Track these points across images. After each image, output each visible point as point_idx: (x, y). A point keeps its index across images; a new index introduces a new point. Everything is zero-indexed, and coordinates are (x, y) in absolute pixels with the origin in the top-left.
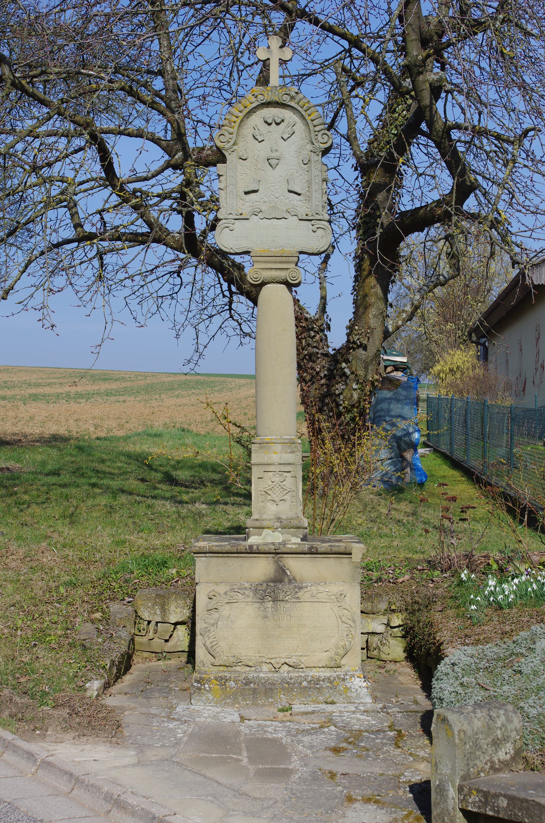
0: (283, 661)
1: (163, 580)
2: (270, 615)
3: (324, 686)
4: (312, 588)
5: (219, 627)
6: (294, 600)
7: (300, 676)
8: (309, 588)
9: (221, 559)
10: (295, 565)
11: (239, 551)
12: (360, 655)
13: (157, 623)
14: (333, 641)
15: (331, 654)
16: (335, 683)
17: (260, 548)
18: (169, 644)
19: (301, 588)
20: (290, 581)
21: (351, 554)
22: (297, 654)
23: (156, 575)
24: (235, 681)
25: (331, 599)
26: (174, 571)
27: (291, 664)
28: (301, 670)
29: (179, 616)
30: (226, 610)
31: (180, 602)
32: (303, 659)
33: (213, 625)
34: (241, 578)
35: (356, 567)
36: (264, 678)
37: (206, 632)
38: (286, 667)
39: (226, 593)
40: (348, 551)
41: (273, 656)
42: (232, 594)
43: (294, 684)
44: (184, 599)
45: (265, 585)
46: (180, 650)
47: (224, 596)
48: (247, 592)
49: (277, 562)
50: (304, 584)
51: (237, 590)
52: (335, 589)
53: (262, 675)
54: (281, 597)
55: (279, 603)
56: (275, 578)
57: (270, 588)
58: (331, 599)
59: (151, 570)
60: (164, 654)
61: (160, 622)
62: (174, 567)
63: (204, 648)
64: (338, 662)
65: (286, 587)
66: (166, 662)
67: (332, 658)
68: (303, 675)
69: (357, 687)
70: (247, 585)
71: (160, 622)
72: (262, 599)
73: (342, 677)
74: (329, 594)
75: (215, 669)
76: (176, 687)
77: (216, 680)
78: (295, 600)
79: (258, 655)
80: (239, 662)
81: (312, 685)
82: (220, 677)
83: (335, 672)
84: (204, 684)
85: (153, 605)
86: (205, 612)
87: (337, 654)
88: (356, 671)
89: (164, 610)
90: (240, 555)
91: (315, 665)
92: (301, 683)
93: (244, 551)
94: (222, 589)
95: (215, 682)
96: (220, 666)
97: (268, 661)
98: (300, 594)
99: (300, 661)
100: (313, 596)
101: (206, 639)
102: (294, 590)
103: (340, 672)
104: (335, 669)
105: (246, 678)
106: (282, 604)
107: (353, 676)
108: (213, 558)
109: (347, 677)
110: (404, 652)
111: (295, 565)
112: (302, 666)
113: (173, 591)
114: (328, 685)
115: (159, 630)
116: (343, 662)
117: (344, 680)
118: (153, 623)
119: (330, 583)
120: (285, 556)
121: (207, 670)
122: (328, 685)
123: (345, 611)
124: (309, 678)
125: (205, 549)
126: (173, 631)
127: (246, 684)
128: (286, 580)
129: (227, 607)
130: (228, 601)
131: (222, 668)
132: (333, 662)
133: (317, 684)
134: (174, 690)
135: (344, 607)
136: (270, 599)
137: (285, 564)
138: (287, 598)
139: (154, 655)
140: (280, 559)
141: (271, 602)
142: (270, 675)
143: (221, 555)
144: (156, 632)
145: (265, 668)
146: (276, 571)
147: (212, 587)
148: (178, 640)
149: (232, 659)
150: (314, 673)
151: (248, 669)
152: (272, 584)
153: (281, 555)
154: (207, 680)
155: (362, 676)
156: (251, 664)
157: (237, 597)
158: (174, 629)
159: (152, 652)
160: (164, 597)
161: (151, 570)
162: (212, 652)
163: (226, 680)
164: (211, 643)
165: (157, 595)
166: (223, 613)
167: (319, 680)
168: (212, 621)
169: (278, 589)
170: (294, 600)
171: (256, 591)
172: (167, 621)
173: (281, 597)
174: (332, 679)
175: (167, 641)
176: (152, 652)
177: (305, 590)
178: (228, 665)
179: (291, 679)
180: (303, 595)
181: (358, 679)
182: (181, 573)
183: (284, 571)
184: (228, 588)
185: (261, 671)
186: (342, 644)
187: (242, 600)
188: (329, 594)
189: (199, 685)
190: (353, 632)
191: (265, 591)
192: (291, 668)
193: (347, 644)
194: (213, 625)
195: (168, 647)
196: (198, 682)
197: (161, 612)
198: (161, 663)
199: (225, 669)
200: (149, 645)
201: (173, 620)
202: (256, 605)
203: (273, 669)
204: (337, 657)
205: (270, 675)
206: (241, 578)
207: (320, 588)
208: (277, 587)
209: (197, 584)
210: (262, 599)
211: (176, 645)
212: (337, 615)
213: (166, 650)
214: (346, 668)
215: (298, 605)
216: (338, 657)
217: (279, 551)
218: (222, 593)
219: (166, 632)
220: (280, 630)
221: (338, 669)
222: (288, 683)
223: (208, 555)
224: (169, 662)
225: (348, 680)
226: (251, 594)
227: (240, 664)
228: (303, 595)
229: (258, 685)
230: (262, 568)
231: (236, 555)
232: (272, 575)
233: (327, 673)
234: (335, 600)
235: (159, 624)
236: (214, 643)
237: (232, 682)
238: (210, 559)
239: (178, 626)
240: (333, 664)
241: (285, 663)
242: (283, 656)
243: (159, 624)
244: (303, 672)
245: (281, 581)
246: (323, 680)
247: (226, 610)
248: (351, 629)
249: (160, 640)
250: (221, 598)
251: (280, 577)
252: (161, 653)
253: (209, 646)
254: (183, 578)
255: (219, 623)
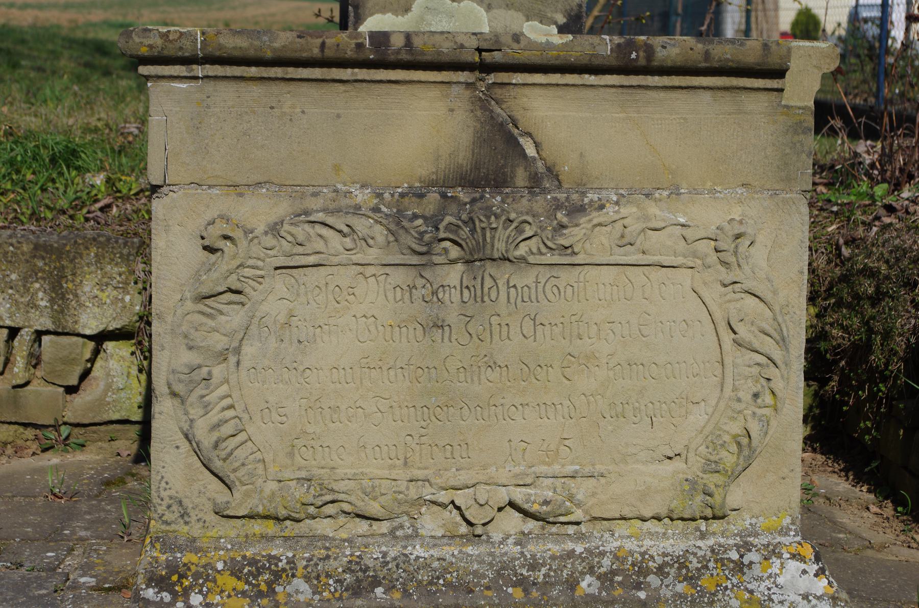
0: (503, 495)
1: (63, 203)
2: (452, 317)
3: (666, 593)
4: (624, 211)
5: (246, 363)
6: (549, 258)
7: (571, 554)
8: (610, 209)
9: (256, 90)
10: (555, 118)
11: (329, 53)
12: (799, 470)
13: (39, 334)
14: (698, 417)
15: (694, 467)
16: (705, 582)
17: (417, 42)
18: (79, 400)
19: (577, 210)
20: (535, 184)
21: (780, 73)
22: (556, 468)
23: (43, 190)
24: (314, 578)
25: (695, 255)
26: (99, 180)
27: (535, 508)
28: (571, 530)
29: (110, 312)
30: (274, 298)
31: (113, 270)
32: (582, 489)
33: (222, 356)
34: (337, 168)
35: (797, 128)
36: (427, 566)
37: (192, 385)
38: (512, 522)
39: (274, 229)
40: (774, 61)
41: (464, 477)
42: (301, 232)
43: (547, 585)
44: (126, 259)
45: (433, 197)
46: (116, 417)
47: (269, 241)
48: (362, 225)
49: (483, 104)
50: (592, 196)
51: (320, 216)
52: (710, 215)
53: (419, 551)
54: (500, 247)
55: (490, 268)
56: (476, 166)
57: (453, 208)
58: (695, 255)
59: (29, 176)
60: (65, 430)
61: (48, 332)
62: (102, 169)
63: (185, 446)
64: (718, 499)
65: (522, 205)
66: (70, 457)
67: (693, 483)
68: (579, 549)
69: (793, 597)
70: (362, 196)
71: (48, 332)
72: (424, 256)
73: (734, 556)
74: (688, 232)
75: (232, 529)
76: (86, 569)
77: (236, 573)
78: (556, 259)
79: (401, 474)
80: (325, 502)
81: (618, 592)
82: (253, 562)
83: (703, 536)
84: (186, 592)
85: (25, 279)
86: (189, 305)
87: (711, 466)
88: (784, 532)
89: (60, 296)
90: (336, 73)
91: (627, 512)
92: (572, 584)
93: (350, 54)
94: (258, 211)
95: (230, 582)
96: (251, 517)
97: (443, 497)
98: (573, 235)
99: (571, 498)
100: (624, 243)
101: (195, 412)
102: (552, 216)
103: (720, 536)
104: (703, 525)
105: (355, 566)
106: (503, 273)
107: (772, 552)
108: (222, 86)
109: (753, 556)
110: (805, 421)
111: (555, 118)
112: (578, 515)
113: (90, 233)
114: (681, 587)
115: (45, 357)
116: (735, 496)
117: (740, 567)
118: (26, 336)
119: (695, 191)
120: (518, 78)
121: (196, 530)
122: (681, 587)
123: (751, 301)
124: (606, 562)
125: (186, 43)
126: (92, 360)
127: (357, 590)
128: (521, 177)
129: (280, 284)
130: (282, 261)
131: (257, 527)
132: (699, 498)
133: (638, 586)
134: (76, 586)
135: (748, 285)
136: (455, 252)
137: (518, 115)
138: (522, 250)
139: (30, 433)
140: (498, 92)
141: (460, 267)
142: (449, 551)
143: (253, 71)
144: (35, 360)
145: (431, 523)
146: (480, 141)
147: (220, 202)
148: (109, 387)
149: (299, 493)
150: (624, 541)
151: (363, 527)
152: (462, 195)
153: (503, 77)
154: (197, 576)
155: (808, 551)
156: (374, 508)
157: (319, 245)
158: (96, 352)
159: (26, 425)
160: (60, 253)
161: (29, 176)
162: (217, 464)
163: (277, 575)
164: (216, 426)
165: (37, 247)
166: (264, 308)
167: (644, 571)
168: (219, 342)
169: (489, 212)
170: (549, 258)
171: (397, 222)
172: (70, 326)
173: (500, 247)
174: (695, 564)
175: (71, 390)
176: (26, 425)
177: (597, 217)
178: (283, 513)
179: (533, 567)
180: (586, 237)
181: (794, 566)
182: (120, 185)
183: (512, 143)
184: (283, 208)
185: (416, 535)
186: (736, 428)
187: (344, 257)
188: (688, 232)
189: (167, 597)
190: (778, 385)
191: (434, 221)
192: (531, 525)
193: (755, 428)
194: (222, 356)
195: (78, 407)
196: (161, 583)
197: (52, 301)
198: (53, 459)
199: (270, 528)
200: (15, 403)
201: (91, 326)
202: (399, 276)
203: (464, 529)
204: (712, 480)
205: (449, 551)
206: (337, 168)
207: (653, 209)
208: (481, 210)
209: (155, 189)
210: (424, 256)
211: (101, 403)
212: (718, 315)
213: (69, 417)
214: (746, 521)
215: (566, 276)
216: (718, 479)
217: (497, 57)
218: (261, 228)
219: (69, 361)
220: (493, 375)
221: (715, 525)
222: (521, 582)
223: (199, 70)
224: (80, 456)
225: (757, 570)
226: (380, 233)
227: (330, 509)
228: (586, 237)
229: (406, 593)
230: (422, 128)
231: (317, 73)
232: (464, 158)
233: (670, 542)
234: (713, 258)
235: (45, 339)
236: (227, 430)
237: (299, 584)
238: (210, 86)
239: (109, 346)
240: (697, 504)
241: (512, 504)
242: (503, 476)
243: (45, 339)
244: (580, 537)
245: (499, 181)
246: (661, 571)
247: (274, 298)
248: (772, 372)
249: (51, 388)
250: (256, 250)
251: (498, 164)
252: (56, 427)
253: (206, 440)
254: (126, 198)
255: (248, 350)
